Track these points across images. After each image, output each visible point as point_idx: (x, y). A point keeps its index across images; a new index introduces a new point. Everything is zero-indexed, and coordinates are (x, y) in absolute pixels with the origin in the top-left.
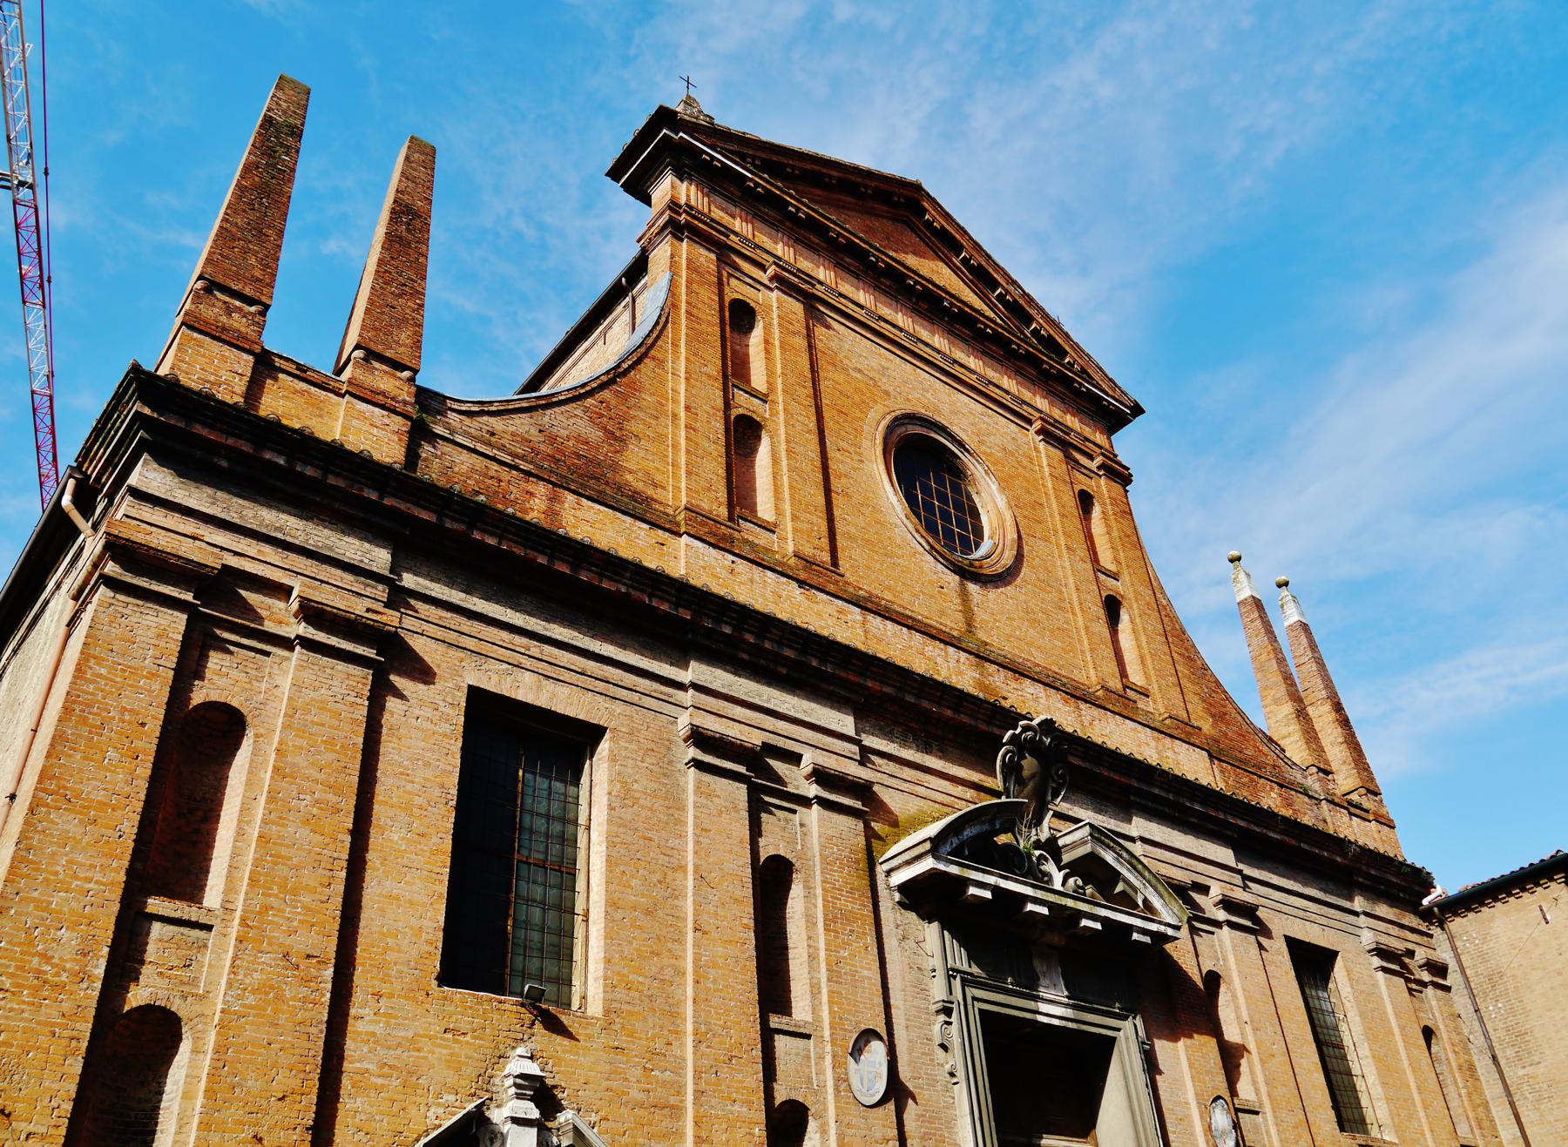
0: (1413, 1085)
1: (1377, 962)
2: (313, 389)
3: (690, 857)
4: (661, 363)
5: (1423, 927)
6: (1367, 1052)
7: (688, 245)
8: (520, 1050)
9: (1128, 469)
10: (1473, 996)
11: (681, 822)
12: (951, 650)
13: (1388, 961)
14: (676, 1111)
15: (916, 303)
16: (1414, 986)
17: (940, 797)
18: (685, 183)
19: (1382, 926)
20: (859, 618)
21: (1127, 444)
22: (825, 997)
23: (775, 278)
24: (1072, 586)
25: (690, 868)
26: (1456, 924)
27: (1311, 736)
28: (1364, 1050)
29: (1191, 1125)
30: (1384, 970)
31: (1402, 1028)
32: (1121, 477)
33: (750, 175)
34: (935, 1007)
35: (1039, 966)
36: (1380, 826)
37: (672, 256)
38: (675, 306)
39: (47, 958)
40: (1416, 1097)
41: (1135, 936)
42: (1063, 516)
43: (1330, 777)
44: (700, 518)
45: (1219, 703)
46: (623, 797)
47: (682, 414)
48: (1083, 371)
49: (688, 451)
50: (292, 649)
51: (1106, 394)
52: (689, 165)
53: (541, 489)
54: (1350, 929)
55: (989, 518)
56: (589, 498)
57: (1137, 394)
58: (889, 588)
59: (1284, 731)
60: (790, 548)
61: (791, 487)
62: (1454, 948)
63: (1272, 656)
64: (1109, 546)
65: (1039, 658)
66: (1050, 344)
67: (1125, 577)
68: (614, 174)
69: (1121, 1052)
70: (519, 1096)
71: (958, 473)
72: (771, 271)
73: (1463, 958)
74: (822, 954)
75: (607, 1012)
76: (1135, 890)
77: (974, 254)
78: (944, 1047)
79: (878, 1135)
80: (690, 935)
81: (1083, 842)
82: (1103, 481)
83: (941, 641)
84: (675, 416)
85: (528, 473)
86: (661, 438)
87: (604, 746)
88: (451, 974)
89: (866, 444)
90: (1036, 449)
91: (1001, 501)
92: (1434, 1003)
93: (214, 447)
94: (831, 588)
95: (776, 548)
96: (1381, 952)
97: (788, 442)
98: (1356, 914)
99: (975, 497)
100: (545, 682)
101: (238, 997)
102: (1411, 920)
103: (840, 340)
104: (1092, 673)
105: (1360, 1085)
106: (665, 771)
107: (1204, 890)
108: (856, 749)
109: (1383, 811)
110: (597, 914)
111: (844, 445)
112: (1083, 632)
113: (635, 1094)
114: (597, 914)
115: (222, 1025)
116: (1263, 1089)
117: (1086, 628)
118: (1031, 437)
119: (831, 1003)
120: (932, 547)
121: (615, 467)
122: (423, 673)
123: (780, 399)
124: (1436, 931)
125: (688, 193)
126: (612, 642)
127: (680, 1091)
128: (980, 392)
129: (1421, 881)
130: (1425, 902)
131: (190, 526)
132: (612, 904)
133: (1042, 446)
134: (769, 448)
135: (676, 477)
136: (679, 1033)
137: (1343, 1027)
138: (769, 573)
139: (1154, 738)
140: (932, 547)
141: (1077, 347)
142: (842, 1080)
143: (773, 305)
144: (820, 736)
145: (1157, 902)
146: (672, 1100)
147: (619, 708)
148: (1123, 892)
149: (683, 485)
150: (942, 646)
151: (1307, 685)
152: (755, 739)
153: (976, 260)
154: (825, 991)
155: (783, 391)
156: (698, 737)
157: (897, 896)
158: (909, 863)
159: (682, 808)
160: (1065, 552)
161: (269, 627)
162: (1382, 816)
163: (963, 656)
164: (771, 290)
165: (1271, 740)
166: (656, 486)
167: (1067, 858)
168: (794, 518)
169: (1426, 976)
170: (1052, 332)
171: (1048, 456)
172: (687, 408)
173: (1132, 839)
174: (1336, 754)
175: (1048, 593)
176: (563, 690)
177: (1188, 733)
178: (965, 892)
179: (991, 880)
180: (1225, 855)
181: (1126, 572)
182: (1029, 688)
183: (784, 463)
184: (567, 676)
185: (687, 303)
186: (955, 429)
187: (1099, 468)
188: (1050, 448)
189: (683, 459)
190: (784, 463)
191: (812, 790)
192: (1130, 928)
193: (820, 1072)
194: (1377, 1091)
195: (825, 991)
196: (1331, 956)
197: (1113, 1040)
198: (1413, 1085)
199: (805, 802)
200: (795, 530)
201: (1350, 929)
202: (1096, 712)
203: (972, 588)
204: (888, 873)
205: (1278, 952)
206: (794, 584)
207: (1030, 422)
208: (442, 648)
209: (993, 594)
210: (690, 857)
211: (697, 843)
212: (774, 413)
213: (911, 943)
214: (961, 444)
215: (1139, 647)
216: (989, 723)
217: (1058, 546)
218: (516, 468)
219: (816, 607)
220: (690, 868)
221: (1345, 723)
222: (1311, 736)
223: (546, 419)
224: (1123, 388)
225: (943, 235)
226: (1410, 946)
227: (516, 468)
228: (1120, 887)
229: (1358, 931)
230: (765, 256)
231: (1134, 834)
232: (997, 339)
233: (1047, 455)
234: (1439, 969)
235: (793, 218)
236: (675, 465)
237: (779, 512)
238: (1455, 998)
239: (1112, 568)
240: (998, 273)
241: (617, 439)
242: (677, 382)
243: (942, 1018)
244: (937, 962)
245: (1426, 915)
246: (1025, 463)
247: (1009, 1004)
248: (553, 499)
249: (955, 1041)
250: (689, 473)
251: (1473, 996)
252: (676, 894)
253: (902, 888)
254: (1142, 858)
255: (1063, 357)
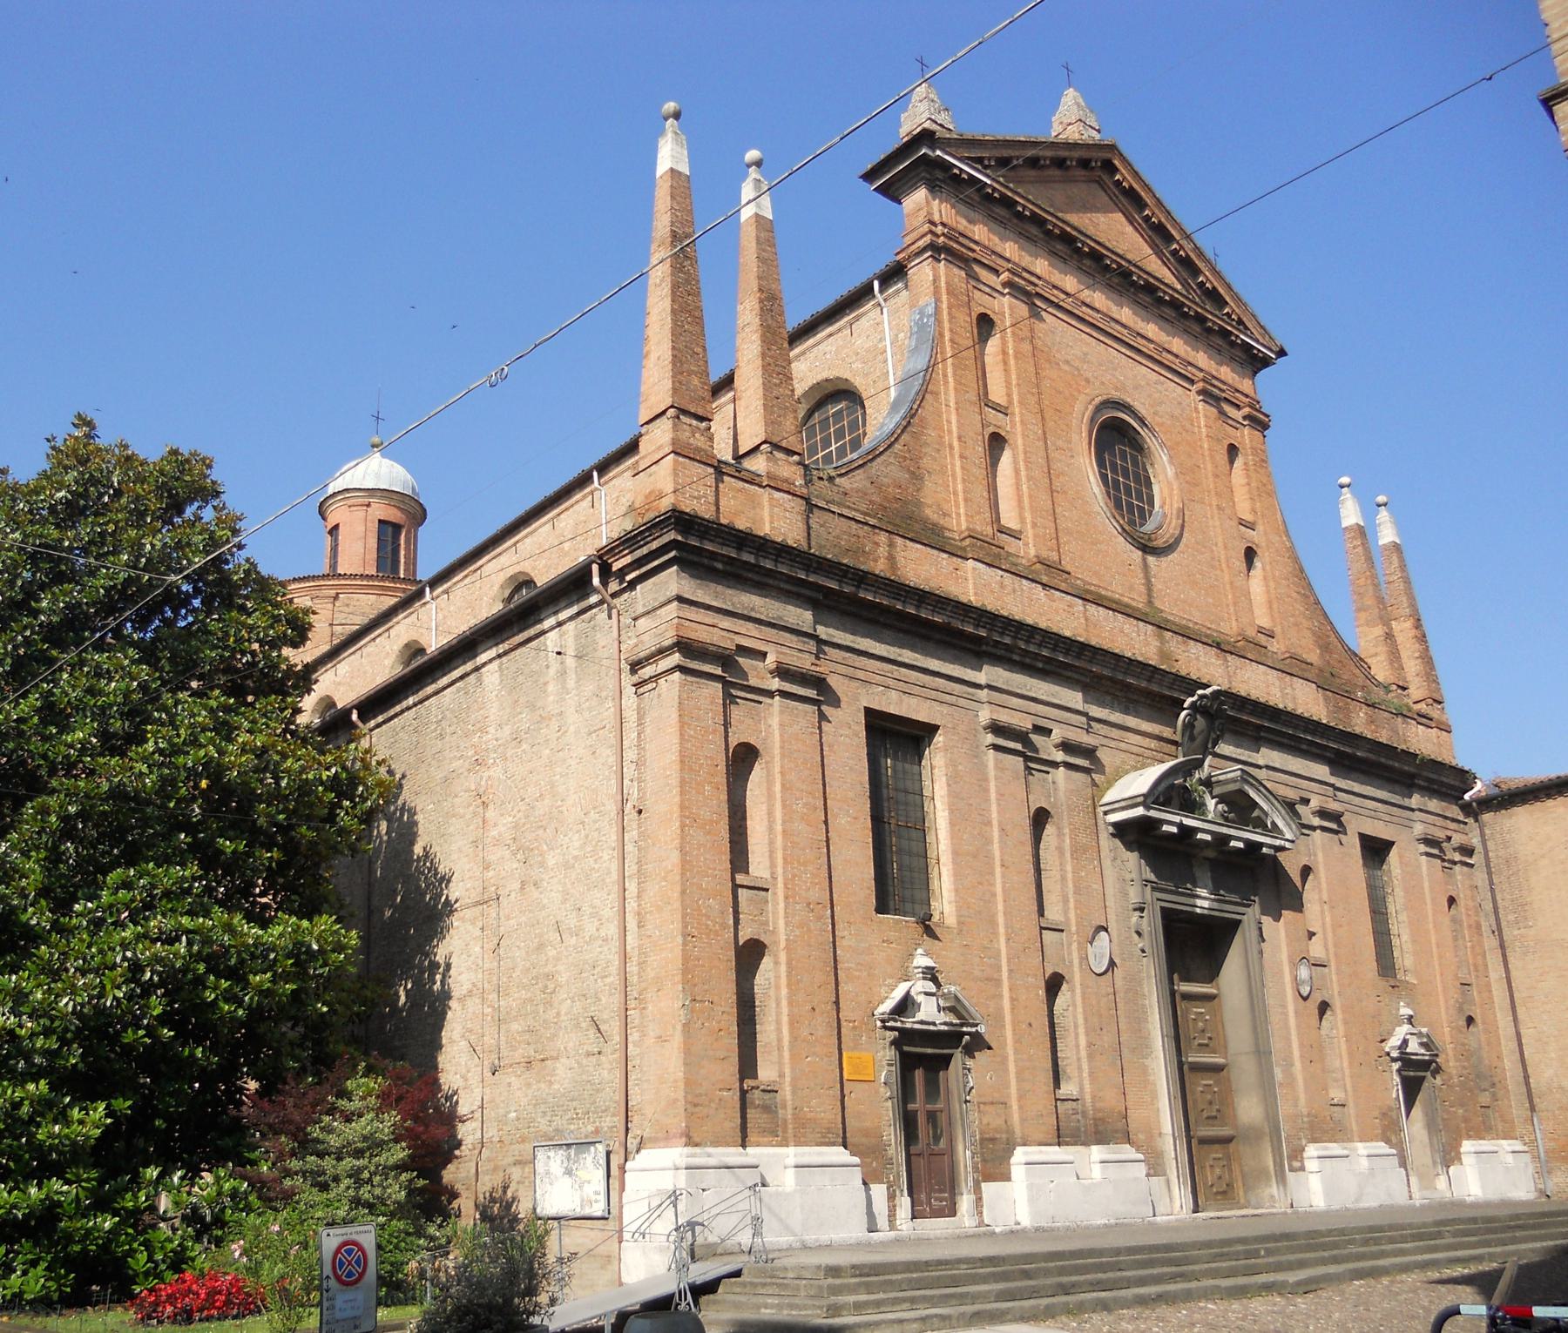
0: (1434, 941)
1: (1423, 848)
2: (747, 485)
3: (994, 815)
4: (936, 394)
5: (1461, 818)
6: (1405, 919)
7: (947, 267)
8: (920, 951)
9: (1268, 416)
10: (1490, 873)
11: (987, 790)
12: (1141, 624)
13: (1432, 847)
14: (998, 982)
15: (1109, 279)
16: (1446, 864)
17: (1135, 750)
18: (937, 201)
19: (1431, 818)
20: (1082, 608)
21: (1268, 386)
22: (1072, 904)
23: (1005, 284)
24: (1220, 544)
25: (995, 822)
26: (1487, 817)
27: (1394, 656)
28: (1403, 917)
29: (1282, 977)
30: (1428, 854)
31: (1433, 900)
32: (1259, 423)
33: (989, 182)
34: (1131, 907)
35: (1198, 873)
36: (1439, 732)
37: (935, 281)
38: (941, 335)
39: (708, 918)
40: (1434, 950)
41: (1265, 850)
42: (1216, 476)
43: (1405, 693)
44: (979, 543)
45: (1327, 635)
46: (953, 779)
47: (956, 443)
48: (1240, 322)
49: (964, 480)
50: (773, 697)
51: (1257, 341)
52: (941, 179)
53: (883, 537)
54: (1406, 822)
55: (1161, 489)
56: (911, 540)
57: (1282, 340)
58: (1096, 573)
59: (1373, 651)
60: (1032, 552)
61: (1030, 496)
62: (1482, 835)
63: (1369, 582)
64: (1247, 496)
65: (1197, 617)
66: (1214, 296)
67: (1260, 527)
68: (869, 176)
69: (1244, 934)
70: (924, 979)
71: (1138, 446)
72: (1005, 276)
73: (1489, 843)
74: (1070, 875)
75: (959, 923)
76: (1266, 814)
77: (1156, 211)
78: (1139, 934)
79: (1103, 992)
80: (998, 870)
81: (1234, 780)
82: (1246, 431)
83: (1135, 618)
84: (951, 447)
85: (873, 527)
86: (943, 468)
87: (939, 739)
88: (882, 908)
89: (1075, 437)
90: (1196, 409)
91: (1170, 471)
92: (1459, 877)
93: (713, 556)
94: (1063, 586)
95: (1022, 554)
96: (1429, 841)
97: (1025, 453)
98: (1413, 810)
99: (1148, 467)
100: (904, 697)
101: (792, 931)
102: (1454, 811)
103: (1053, 326)
104: (1234, 624)
105: (1395, 941)
106: (976, 755)
107: (1306, 801)
108: (1084, 719)
109: (1444, 718)
110: (946, 859)
111: (1060, 443)
112: (1228, 587)
113: (977, 973)
114: (946, 859)
115: (787, 948)
116: (1332, 950)
117: (1231, 583)
118: (1193, 397)
119: (1076, 908)
120: (1123, 529)
121: (919, 504)
122: (835, 702)
123: (1017, 410)
124: (1470, 820)
125: (942, 210)
126: (913, 649)
127: (999, 970)
128: (1157, 360)
129: (1464, 778)
130: (1467, 797)
131: (710, 618)
132: (956, 853)
133: (1201, 406)
134: (1011, 460)
135: (957, 506)
136: (996, 934)
137: (1390, 899)
138: (1024, 581)
139: (1278, 678)
140: (1123, 529)
141: (1238, 299)
142: (1084, 958)
143: (1006, 308)
144: (1069, 715)
145: (1280, 823)
146: (995, 976)
147: (945, 709)
148: (1258, 817)
149: (962, 511)
150: (1135, 622)
151: (1393, 601)
152: (729, 643)
153: (1158, 217)
154: (1072, 900)
155: (1019, 402)
156: (997, 728)
157: (1111, 829)
158: (1123, 809)
159: (986, 780)
160: (1216, 511)
161: (753, 682)
162: (1442, 723)
163: (1150, 627)
164: (1003, 295)
165: (1356, 655)
166: (945, 515)
167: (1217, 791)
168: (1034, 525)
169: (1457, 857)
170: (1216, 284)
171: (1206, 416)
172: (959, 438)
173: (1260, 767)
174: (1412, 667)
175: (1202, 553)
176: (913, 701)
177: (1303, 670)
178: (1160, 828)
179: (1177, 819)
180: (1321, 771)
181: (1260, 522)
182: (1195, 649)
183: (1023, 473)
184: (916, 690)
185: (951, 330)
186: (1137, 406)
187: (1245, 418)
188: (1208, 407)
189: (960, 487)
190: (1023, 473)
191: (1059, 756)
192: (1261, 845)
193: (1070, 954)
194: (1408, 947)
195: (1072, 900)
196: (1388, 845)
197: (1240, 921)
198: (1434, 941)
199: (1055, 765)
200: (1036, 536)
201: (1406, 822)
202: (1239, 661)
203: (1151, 559)
204: (1106, 813)
205: (1353, 846)
206: (1040, 587)
207: (1192, 382)
208: (846, 681)
209: (1166, 561)
210: (994, 815)
211: (999, 805)
212: (1013, 424)
213: (1119, 862)
214: (1142, 421)
215: (1268, 592)
216: (1170, 688)
217: (1211, 505)
218: (866, 524)
219: (1055, 605)
220: (995, 822)
221: (1422, 639)
222: (1394, 656)
223: (874, 471)
224: (1273, 335)
225: (1131, 194)
226: (1449, 833)
227: (866, 524)
228: (1256, 813)
229: (1411, 824)
230: (1000, 261)
231: (1261, 762)
232: (1175, 305)
233: (1204, 412)
234: (1468, 851)
235: (1020, 216)
236: (955, 493)
237: (1022, 520)
238: (1477, 873)
239: (1248, 517)
240: (1175, 228)
241: (916, 477)
242: (948, 412)
243: (1138, 913)
244: (1134, 875)
245: (1467, 809)
246: (1188, 426)
247: (1177, 902)
248: (891, 545)
249: (1145, 928)
250: (966, 500)
251: (1490, 873)
252: (989, 841)
253: (1116, 825)
254: (1265, 783)
255: (1221, 309)
